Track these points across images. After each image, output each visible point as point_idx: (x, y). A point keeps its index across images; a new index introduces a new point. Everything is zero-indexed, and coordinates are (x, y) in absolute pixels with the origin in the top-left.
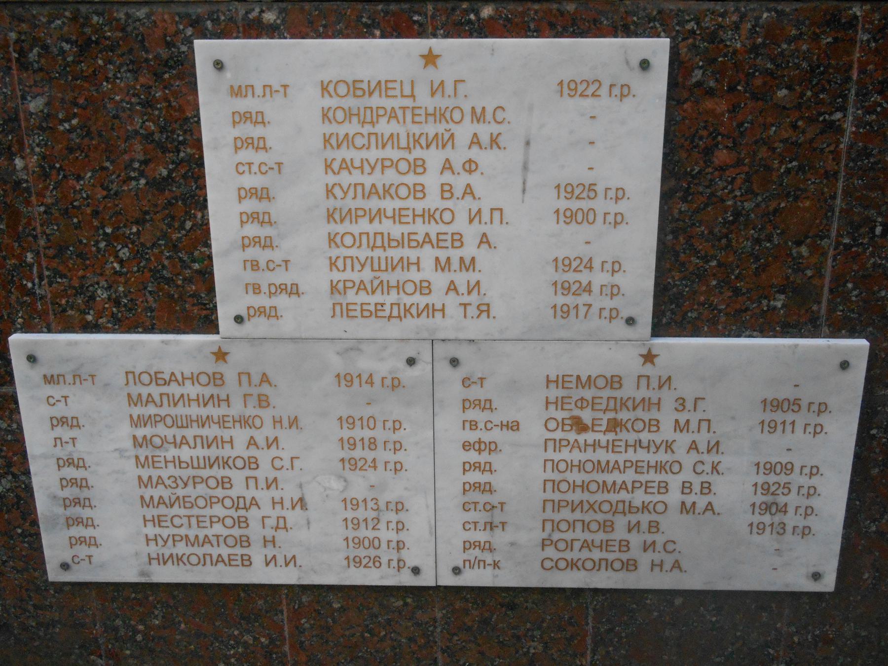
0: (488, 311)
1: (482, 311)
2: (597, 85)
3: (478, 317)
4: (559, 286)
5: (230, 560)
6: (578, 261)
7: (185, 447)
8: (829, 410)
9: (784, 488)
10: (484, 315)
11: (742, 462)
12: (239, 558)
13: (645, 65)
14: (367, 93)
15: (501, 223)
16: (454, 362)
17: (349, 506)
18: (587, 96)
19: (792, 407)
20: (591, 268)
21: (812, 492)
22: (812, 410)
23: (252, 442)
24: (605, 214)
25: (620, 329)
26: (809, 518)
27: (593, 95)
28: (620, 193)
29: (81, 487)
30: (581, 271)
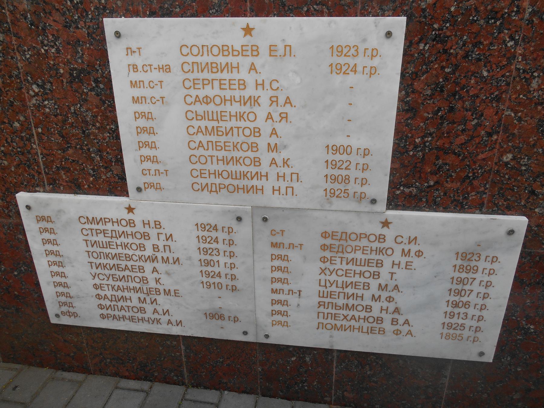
0: (287, 117)
1: (282, 118)
2: (348, 163)
3: (280, 121)
4: (329, 177)
5: (132, 268)
6: (347, 66)
7: (119, 291)
8: (487, 308)
9: (461, 326)
10: (284, 120)
11: (438, 284)
12: (137, 267)
13: (389, 34)
14: (220, 70)
15: (293, 195)
16: (265, 220)
17: (200, 228)
18: (349, 56)
19: (458, 338)
20: (355, 71)
21: (488, 285)
22: (476, 308)
23: (155, 311)
24: (356, 178)
25: (365, 207)
26: (483, 311)
27: (346, 169)
28: (364, 181)
29: (69, 306)
30: (348, 74)
